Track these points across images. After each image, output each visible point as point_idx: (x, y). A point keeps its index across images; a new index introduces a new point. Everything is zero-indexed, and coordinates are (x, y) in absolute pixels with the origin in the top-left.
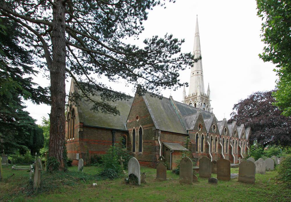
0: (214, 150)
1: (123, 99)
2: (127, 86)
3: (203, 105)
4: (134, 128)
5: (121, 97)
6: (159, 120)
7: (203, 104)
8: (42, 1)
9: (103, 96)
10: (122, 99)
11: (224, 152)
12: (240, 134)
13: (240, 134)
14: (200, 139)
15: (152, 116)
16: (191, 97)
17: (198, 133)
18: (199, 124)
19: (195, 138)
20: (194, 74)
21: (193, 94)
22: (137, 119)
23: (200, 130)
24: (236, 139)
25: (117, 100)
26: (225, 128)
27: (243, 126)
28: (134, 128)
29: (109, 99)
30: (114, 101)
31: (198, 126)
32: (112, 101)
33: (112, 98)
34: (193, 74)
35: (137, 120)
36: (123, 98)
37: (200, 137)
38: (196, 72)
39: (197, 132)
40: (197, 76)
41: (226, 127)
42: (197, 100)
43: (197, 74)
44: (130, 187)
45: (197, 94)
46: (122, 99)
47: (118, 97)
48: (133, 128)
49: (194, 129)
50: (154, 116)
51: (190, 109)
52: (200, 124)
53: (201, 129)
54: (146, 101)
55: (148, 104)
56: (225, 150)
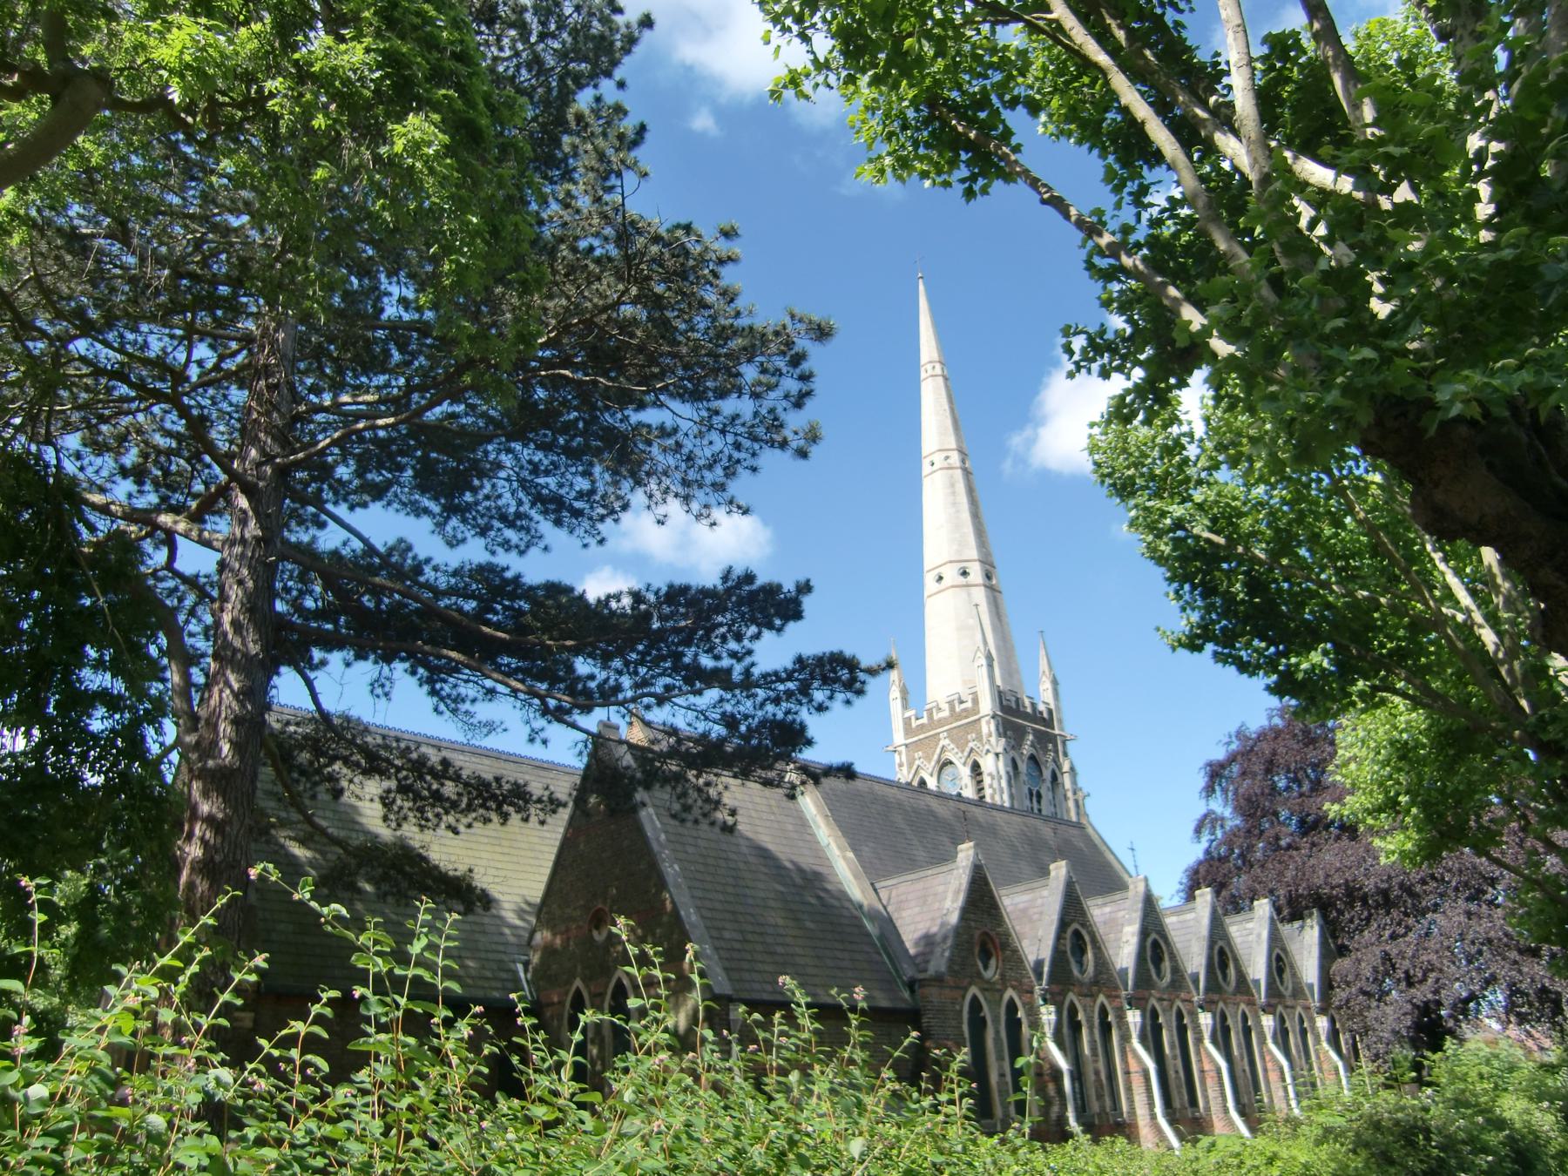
0: (1100, 1097)
1: (515, 818)
2: (538, 741)
3: (1029, 774)
4: (578, 983)
5: (499, 807)
6: (727, 935)
7: (1023, 767)
8: (365, 1169)
9: (394, 801)
10: (505, 818)
11: (1177, 1104)
12: (1257, 969)
13: (1257, 969)
14: (997, 1032)
15: (688, 916)
16: (942, 722)
17: (983, 990)
18: (977, 933)
19: (965, 1028)
20: (946, 583)
21: (951, 703)
22: (597, 928)
23: (988, 974)
24: (1238, 1005)
25: (476, 824)
26: (1149, 941)
27: (1263, 907)
28: (578, 983)
29: (427, 820)
30: (456, 832)
31: (977, 950)
32: (449, 827)
33: (447, 813)
34: (941, 578)
35: (595, 933)
36: (511, 809)
37: (996, 1020)
38: (956, 567)
39: (973, 990)
40: (962, 593)
41: (1154, 936)
42: (979, 738)
43: (962, 580)
44: (1313, 845)
45: (976, 701)
46: (505, 818)
47: (483, 806)
48: (569, 982)
49: (950, 968)
50: (698, 908)
51: (932, 813)
52: (986, 934)
53: (993, 962)
54: (650, 816)
55: (663, 837)
56: (1179, 1087)
